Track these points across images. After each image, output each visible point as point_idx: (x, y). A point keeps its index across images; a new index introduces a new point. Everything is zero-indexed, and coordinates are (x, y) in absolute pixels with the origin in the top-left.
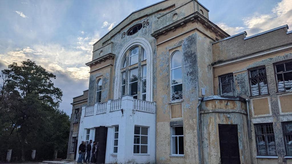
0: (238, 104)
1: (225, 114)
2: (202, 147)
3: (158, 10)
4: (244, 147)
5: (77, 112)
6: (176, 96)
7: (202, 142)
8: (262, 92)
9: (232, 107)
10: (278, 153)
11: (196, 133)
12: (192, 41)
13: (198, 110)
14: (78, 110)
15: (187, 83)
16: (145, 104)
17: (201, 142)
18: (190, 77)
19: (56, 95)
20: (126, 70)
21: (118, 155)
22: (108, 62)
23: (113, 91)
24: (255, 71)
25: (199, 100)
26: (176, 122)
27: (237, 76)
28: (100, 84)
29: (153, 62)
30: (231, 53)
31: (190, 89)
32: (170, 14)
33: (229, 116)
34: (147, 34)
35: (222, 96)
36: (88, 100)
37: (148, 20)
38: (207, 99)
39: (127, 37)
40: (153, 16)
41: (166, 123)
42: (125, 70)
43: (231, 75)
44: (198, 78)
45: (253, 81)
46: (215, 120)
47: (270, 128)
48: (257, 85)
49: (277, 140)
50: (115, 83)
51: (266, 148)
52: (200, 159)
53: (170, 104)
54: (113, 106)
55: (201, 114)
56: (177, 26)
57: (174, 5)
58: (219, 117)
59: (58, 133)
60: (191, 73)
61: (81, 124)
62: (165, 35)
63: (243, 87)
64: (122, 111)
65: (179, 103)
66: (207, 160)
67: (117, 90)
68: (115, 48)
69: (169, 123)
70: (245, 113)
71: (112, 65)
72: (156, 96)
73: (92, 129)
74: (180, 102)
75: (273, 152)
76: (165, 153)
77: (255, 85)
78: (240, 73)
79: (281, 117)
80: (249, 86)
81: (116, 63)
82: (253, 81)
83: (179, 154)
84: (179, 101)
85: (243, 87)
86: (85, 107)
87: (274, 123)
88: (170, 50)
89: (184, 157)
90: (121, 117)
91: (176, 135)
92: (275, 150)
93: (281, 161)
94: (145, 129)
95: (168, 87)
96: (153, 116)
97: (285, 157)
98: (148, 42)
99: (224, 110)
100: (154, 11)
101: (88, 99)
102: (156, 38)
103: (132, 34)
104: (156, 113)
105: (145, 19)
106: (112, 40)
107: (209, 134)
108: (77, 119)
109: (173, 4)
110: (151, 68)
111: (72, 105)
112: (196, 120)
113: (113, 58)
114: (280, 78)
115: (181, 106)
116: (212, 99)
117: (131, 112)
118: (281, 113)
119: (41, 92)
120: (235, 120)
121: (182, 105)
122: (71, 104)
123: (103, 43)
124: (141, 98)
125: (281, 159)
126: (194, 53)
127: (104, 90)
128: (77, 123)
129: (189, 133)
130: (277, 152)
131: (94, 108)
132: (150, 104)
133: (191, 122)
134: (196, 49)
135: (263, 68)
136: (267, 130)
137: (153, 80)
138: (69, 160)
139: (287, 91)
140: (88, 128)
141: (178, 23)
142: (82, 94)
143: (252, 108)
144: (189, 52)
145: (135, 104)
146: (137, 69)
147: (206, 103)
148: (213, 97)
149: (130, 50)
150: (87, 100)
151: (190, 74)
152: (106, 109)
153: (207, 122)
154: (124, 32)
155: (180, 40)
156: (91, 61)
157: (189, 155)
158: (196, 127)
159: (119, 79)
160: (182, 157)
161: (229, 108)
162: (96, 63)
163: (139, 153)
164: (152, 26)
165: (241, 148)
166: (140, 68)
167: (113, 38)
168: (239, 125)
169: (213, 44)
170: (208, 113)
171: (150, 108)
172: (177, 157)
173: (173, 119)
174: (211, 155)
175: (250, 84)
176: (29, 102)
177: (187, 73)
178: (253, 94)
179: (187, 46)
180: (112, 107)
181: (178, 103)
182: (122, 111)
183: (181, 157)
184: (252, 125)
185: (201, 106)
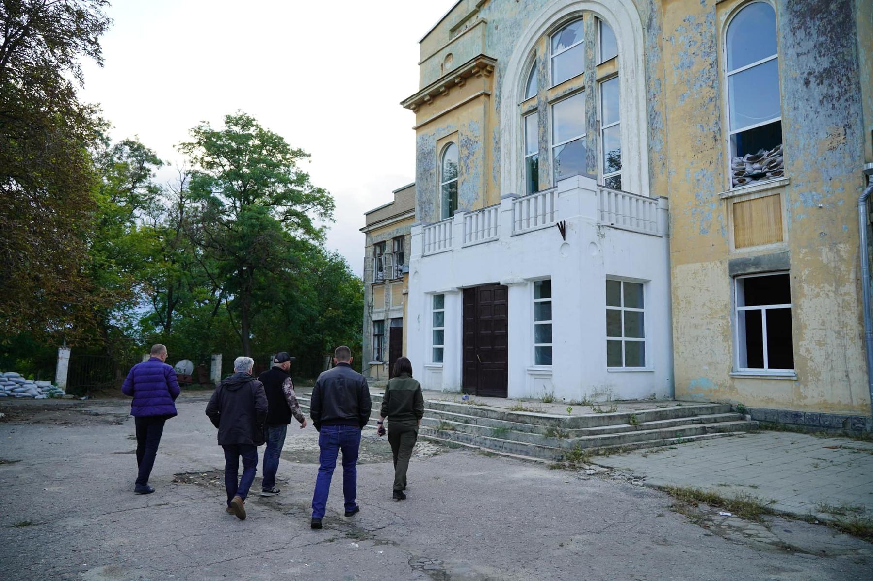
13: (862, 209)
15: (807, 116)
16: (630, 203)
18: (817, 90)
19: (319, 207)
21: (554, 373)
22: (475, 87)
23: (497, 179)
26: (757, 262)
28: (452, 155)
29: (647, 62)
31: (823, 135)
36: (417, 212)
42: (534, 103)
44: (860, 89)
53: (727, 198)
54: (536, 210)
59: (331, 312)
64: (563, 230)
65: (769, 193)
67: (509, 172)
68: (495, 39)
69: (727, 265)
71: (488, 95)
72: (662, 178)
73: (451, 292)
74: (772, 189)
76: (710, 364)
81: (500, 88)
83: (770, 367)
84: (769, 186)
86: (420, 227)
89: (795, 379)
90: (559, 252)
91: (746, 305)
95: (716, 140)
96: (659, 245)
101: (417, 208)
106: (482, 15)
111: (364, 235)
113: (491, 73)
117: (592, 233)
119: (278, 200)
123: (453, 30)
127: (465, 176)
129: (818, 295)
140: (439, 290)
142: (391, 198)
146: (581, 97)
149: (549, 35)
150: (413, 214)
152: (496, 227)
156: (418, 91)
157: (820, 372)
160: (788, 379)
162: (435, 96)
163: (621, 365)
166: (592, 90)
172: (763, 378)
173: (738, 251)
176: (252, 226)
180: (517, 218)
182: (563, 230)
183: (779, 378)
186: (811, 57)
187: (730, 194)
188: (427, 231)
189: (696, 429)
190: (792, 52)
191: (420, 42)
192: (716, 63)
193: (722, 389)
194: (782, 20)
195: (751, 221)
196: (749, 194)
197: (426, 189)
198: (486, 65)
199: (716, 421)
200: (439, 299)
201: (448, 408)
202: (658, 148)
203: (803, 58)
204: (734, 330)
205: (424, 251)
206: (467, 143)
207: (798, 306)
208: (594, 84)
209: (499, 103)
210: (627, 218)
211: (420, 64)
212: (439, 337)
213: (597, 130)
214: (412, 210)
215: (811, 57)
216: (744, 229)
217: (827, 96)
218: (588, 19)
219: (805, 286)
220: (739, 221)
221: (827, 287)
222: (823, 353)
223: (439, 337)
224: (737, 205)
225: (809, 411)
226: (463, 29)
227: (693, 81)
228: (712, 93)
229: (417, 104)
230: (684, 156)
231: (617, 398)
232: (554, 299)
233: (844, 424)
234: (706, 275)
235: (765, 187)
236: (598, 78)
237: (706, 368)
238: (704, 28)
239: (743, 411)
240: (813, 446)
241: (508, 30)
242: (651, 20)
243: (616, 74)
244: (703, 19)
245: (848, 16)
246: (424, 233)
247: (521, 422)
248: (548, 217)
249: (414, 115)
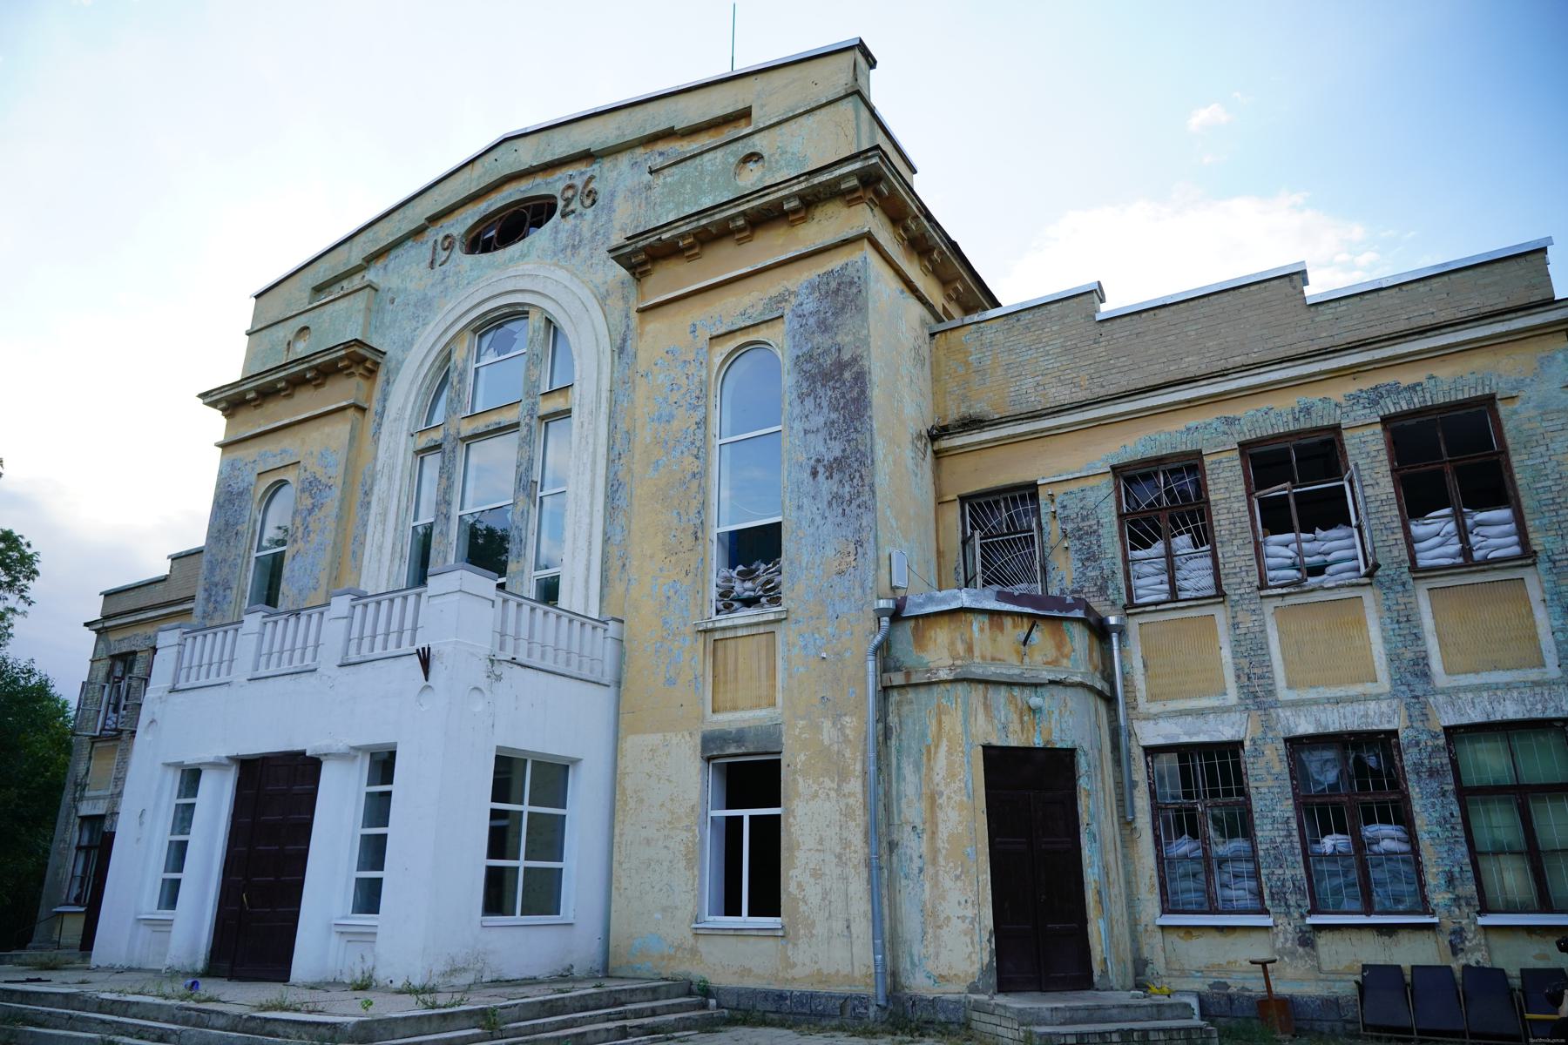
0: (1079, 639)
1: (1016, 691)
2: (891, 872)
3: (650, 130)
4: (1105, 869)
5: (122, 671)
6: (742, 588)
7: (892, 846)
8: (1185, 584)
9: (1052, 653)
10: (1273, 899)
11: (860, 796)
12: (844, 296)
13: (871, 665)
14: (126, 659)
17: (884, 844)
18: (827, 486)
20: (445, 437)
22: (340, 392)
23: (357, 556)
24: (1147, 477)
25: (880, 612)
26: (739, 737)
27: (1057, 500)
29: (613, 403)
30: (1030, 382)
31: (830, 552)
32: (719, 153)
33: (1035, 701)
34: (584, 252)
35: (1001, 597)
36: (198, 606)
37: (591, 178)
38: (921, 605)
39: (465, 262)
40: (624, 160)
41: (674, 741)
42: (437, 436)
43: (1028, 492)
44: (874, 492)
45: (1140, 529)
46: (966, 721)
47: (1224, 767)
48: (1158, 548)
49: (1265, 832)
50: (375, 508)
51: (1209, 872)
52: (878, 942)
53: (705, 631)
55: (886, 690)
56: (766, 216)
57: (745, 114)
58: (986, 707)
60: (837, 466)
61: (146, 731)
62: (690, 258)
63: (1090, 557)
64: (425, 659)
65: (762, 629)
66: (917, 949)
67: (380, 548)
68: (388, 319)
69: (698, 740)
71: (362, 410)
72: (619, 588)
73: (216, 765)
75: (1240, 893)
76: (664, 910)
77: (1149, 546)
78: (1074, 487)
79: (1284, 713)
80: (1120, 555)
81: (385, 400)
82: (1140, 529)
83: (751, 914)
84: (761, 619)
85: (1090, 557)
86: (177, 632)
87: (1247, 743)
88: (718, 337)
89: (780, 933)
90: (411, 704)
91: (728, 808)
92: (1253, 884)
93: (1286, 940)
94: (555, 777)
96: (599, 701)
97: (1309, 921)
98: (586, 294)
99: (1012, 670)
100: (631, 134)
101: (200, 595)
102: (633, 274)
103: (496, 249)
104: (619, 683)
105: (576, 174)
106: (371, 275)
107: (933, 799)
108: (116, 710)
109: (740, 106)
110: (596, 429)
111: (94, 635)
112: (858, 723)
113: (371, 373)
114: (1275, 518)
115: (772, 647)
116: (954, 606)
117: (477, 672)
118: (1284, 694)
120: (1066, 723)
121: (779, 637)
122: (86, 624)
123: (318, 289)
125: (1285, 931)
127: (300, 544)
128: (118, 737)
130: (1266, 892)
131: (234, 641)
132: (588, 628)
133: (828, 733)
134: (866, 342)
135: (1190, 465)
136: (1212, 781)
137: (607, 496)
138: (46, 956)
139: (1312, 580)
140: (190, 759)
141: (771, 197)
142: (162, 568)
143: (1138, 664)
145: (504, 622)
146: (512, 439)
147: (917, 626)
148: (955, 598)
149: (475, 331)
151: (830, 470)
152: (317, 646)
153: (924, 735)
154: (447, 237)
155: (773, 292)
158: (856, 762)
159: (397, 487)
160: (769, 933)
161: (1038, 658)
163: (514, 914)
164: (611, 210)
165: (1091, 875)
167: (380, 263)
168: (1086, 754)
169: (932, 335)
170: (930, 684)
171: (586, 652)
172: (738, 933)
173: (720, 717)
174: (942, 917)
175: (1124, 545)
177: (812, 462)
178: (1140, 592)
179: (812, 321)
180: (355, 633)
181: (754, 630)
182: (425, 659)
184: (1138, 753)
185: (889, 648)
187: (710, 625)
188: (190, 641)
189: (608, 1030)
190: (797, 425)
191: (257, 297)
192: (703, 423)
193: (679, 955)
194: (788, 380)
195: (736, 670)
196: (735, 627)
197: (224, 560)
198: (365, 359)
199: (654, 1012)
200: (191, 778)
201: (134, 1010)
202: (618, 538)
203: (811, 437)
204: (702, 850)
205: (176, 678)
206: (312, 486)
207: (790, 812)
208: (534, 422)
209: (380, 425)
210: (550, 651)
211: (249, 334)
212: (178, 854)
213: (531, 496)
214: (192, 598)
216: (726, 683)
217: (837, 497)
218: (535, 320)
219: (800, 780)
220: (721, 669)
221: (828, 783)
222: (819, 888)
223: (178, 854)
224: (720, 644)
225: (797, 988)
226: (336, 291)
227: (671, 443)
228: (695, 466)
229: (230, 401)
230: (652, 557)
231: (495, 977)
232: (397, 788)
233: (842, 1008)
234: (669, 753)
235: (755, 620)
236: (541, 413)
237: (658, 916)
238: (692, 369)
239: (706, 991)
241: (412, 309)
242: (624, 341)
243: (566, 413)
244: (691, 356)
245: (863, 392)
246: (181, 645)
247: (269, 1034)
248: (407, 636)
249: (224, 421)
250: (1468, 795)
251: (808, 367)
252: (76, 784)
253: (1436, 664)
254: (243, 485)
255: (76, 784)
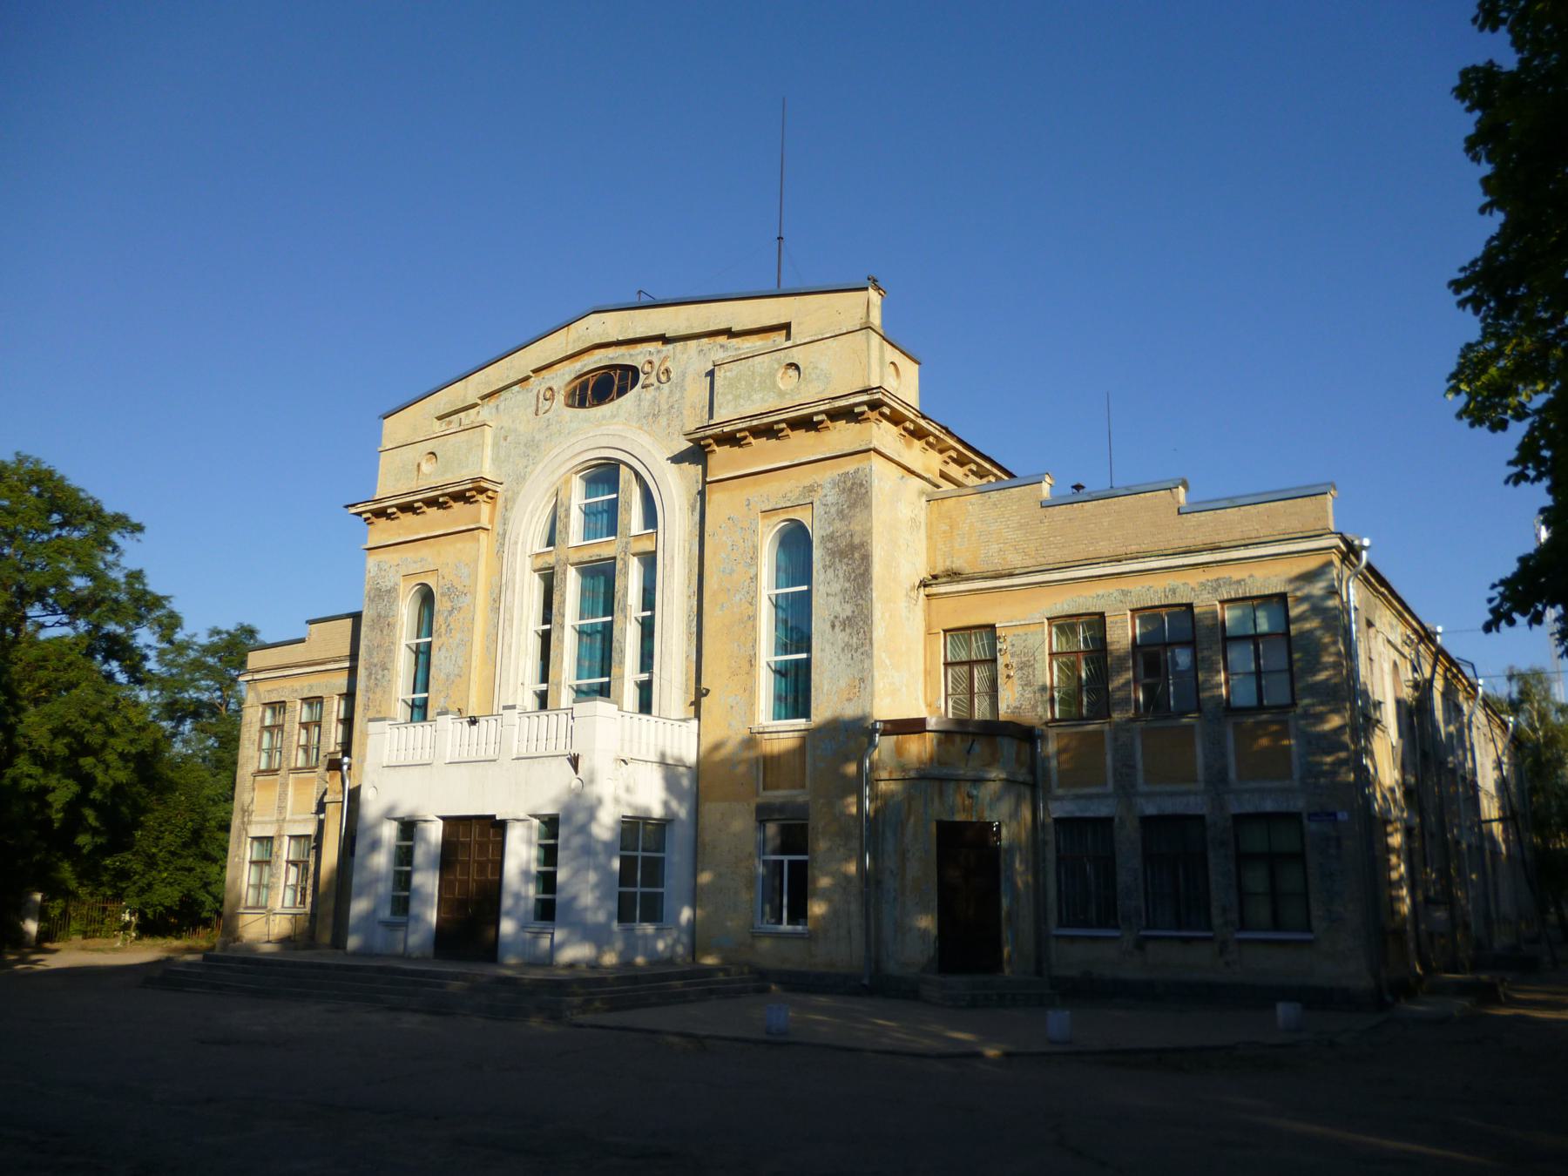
34: (663, 421)
37: (666, 358)
60: (848, 623)
70: (1029, 778)
78: (1020, 631)
97: (1142, 933)
109: (783, 321)
118: (1142, 787)
124: (630, 696)
126: (862, 545)
127: (444, 638)
134: (870, 532)
144: (843, 535)
164: (683, 389)
173: (770, 793)
179: (833, 510)
186: (837, 599)
198: (487, 490)
203: (831, 599)
215: (837, 599)
217: (848, 645)
240: (269, 641)
250: (1243, 859)
251: (830, 545)
252: (244, 811)
253: (1232, 775)
254: (390, 585)
255: (244, 811)
